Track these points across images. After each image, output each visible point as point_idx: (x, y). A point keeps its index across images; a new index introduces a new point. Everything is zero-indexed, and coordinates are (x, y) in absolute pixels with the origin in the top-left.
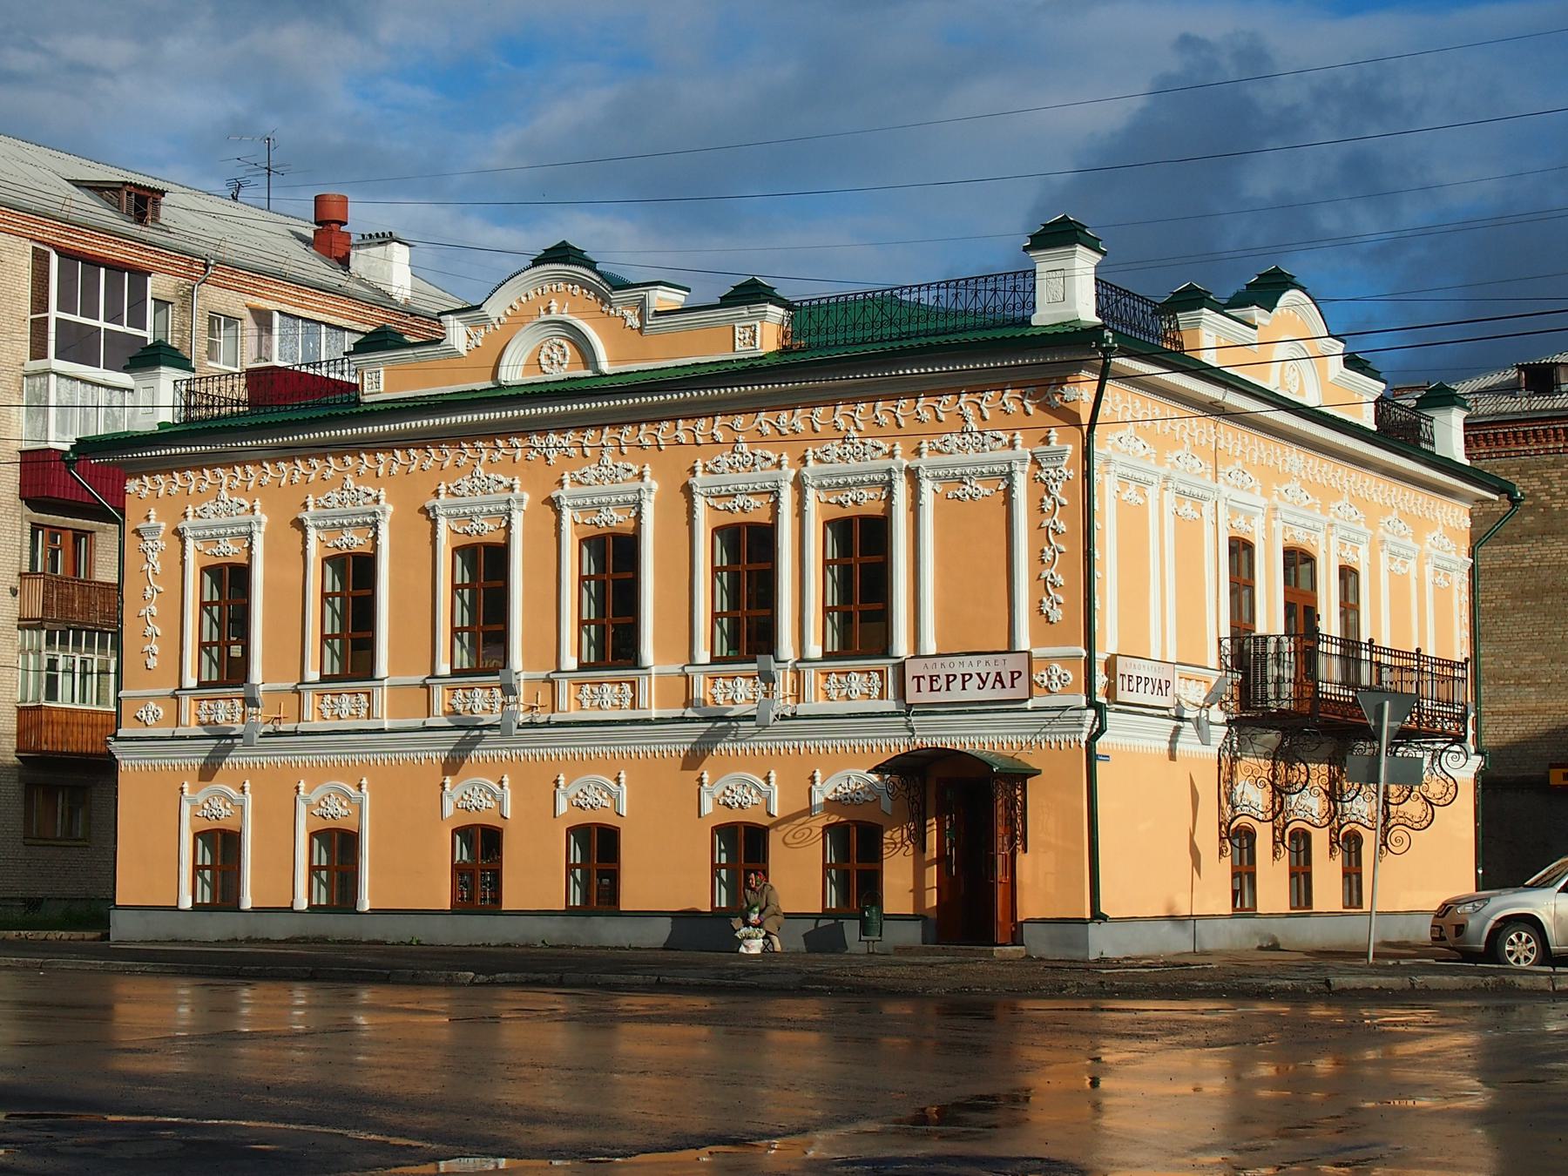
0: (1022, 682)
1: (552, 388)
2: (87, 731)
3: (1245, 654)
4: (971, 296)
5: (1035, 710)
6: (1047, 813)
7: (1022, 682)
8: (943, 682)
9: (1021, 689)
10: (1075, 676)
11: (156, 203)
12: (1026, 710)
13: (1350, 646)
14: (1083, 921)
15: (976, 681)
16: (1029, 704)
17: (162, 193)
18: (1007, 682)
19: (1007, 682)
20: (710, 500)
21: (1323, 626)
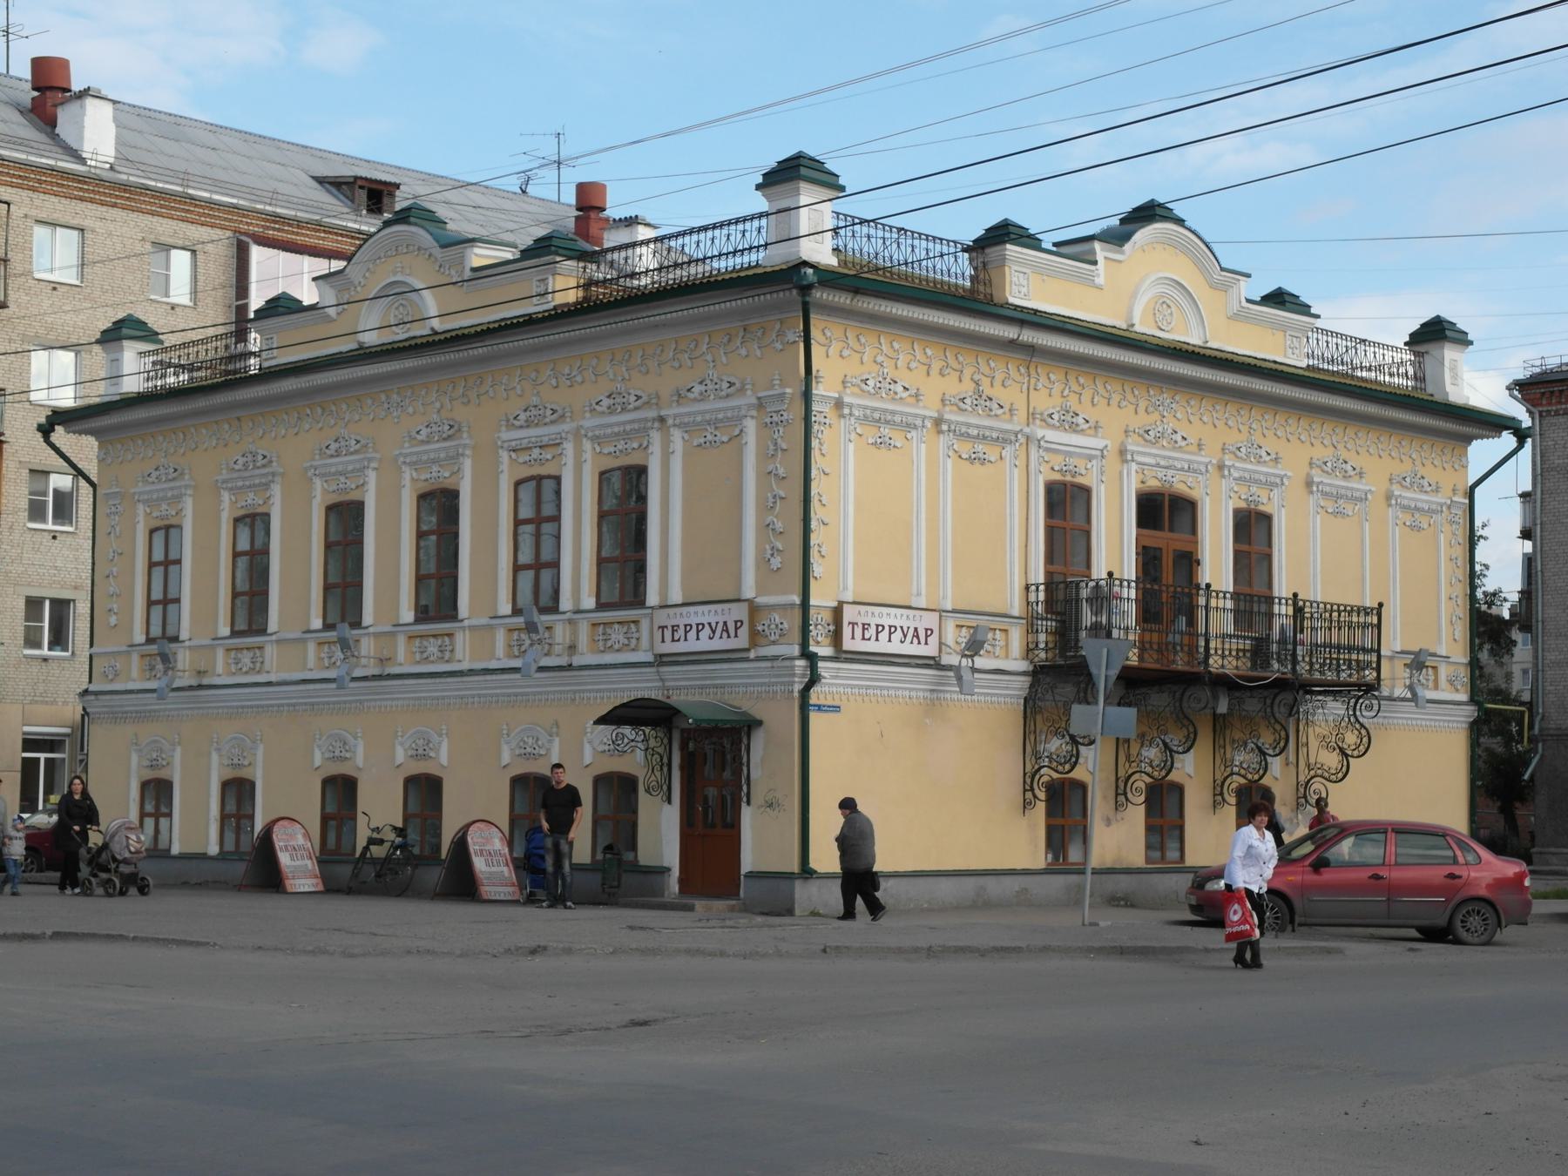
0: (933, 640)
1: (419, 341)
2: (652, 743)
3: (1064, 599)
4: (739, 236)
5: (758, 659)
6: (765, 762)
7: (744, 632)
8: (681, 631)
9: (742, 641)
10: (792, 622)
11: (392, 195)
12: (747, 660)
13: (1253, 599)
14: (788, 876)
15: (707, 631)
16: (752, 655)
17: (397, 186)
18: (732, 633)
19: (732, 633)
20: (514, 455)
21: (1206, 575)
